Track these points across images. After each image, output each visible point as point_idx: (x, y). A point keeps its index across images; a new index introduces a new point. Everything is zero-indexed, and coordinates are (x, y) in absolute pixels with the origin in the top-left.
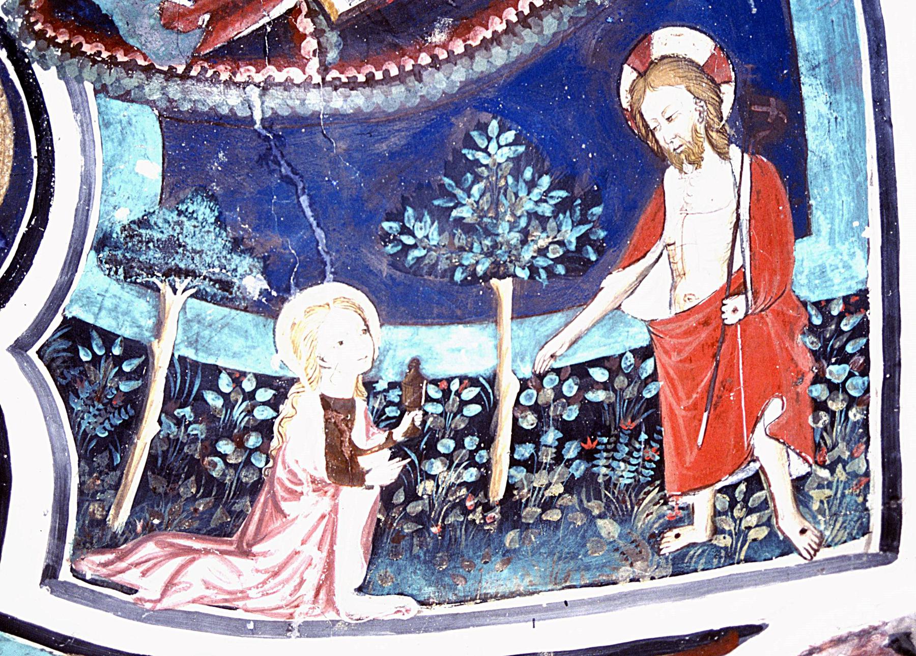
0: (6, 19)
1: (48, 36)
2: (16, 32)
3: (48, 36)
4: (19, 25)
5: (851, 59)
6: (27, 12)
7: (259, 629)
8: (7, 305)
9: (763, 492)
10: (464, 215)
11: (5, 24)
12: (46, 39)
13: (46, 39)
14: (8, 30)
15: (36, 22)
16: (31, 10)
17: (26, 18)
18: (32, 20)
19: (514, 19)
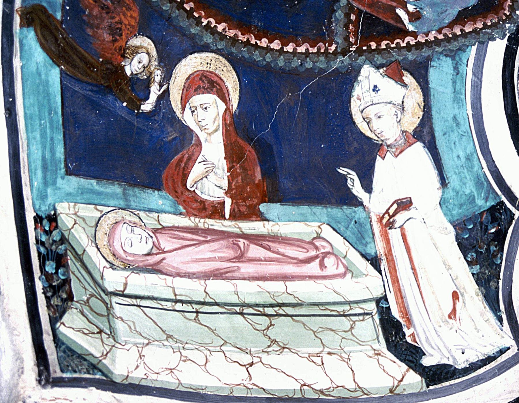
0: (508, 35)
1: (511, 4)
2: (514, 26)
3: (511, 4)
4: (509, 25)
5: (62, 67)
6: (501, 23)
7: (455, 284)
8: (517, 153)
9: (58, 370)
10: (57, 373)
11: (511, 34)
12: (513, 4)
13: (513, 4)
14: (514, 32)
15: (505, 14)
16: (499, 21)
17: (504, 21)
18: (504, 18)
19: (459, 33)
